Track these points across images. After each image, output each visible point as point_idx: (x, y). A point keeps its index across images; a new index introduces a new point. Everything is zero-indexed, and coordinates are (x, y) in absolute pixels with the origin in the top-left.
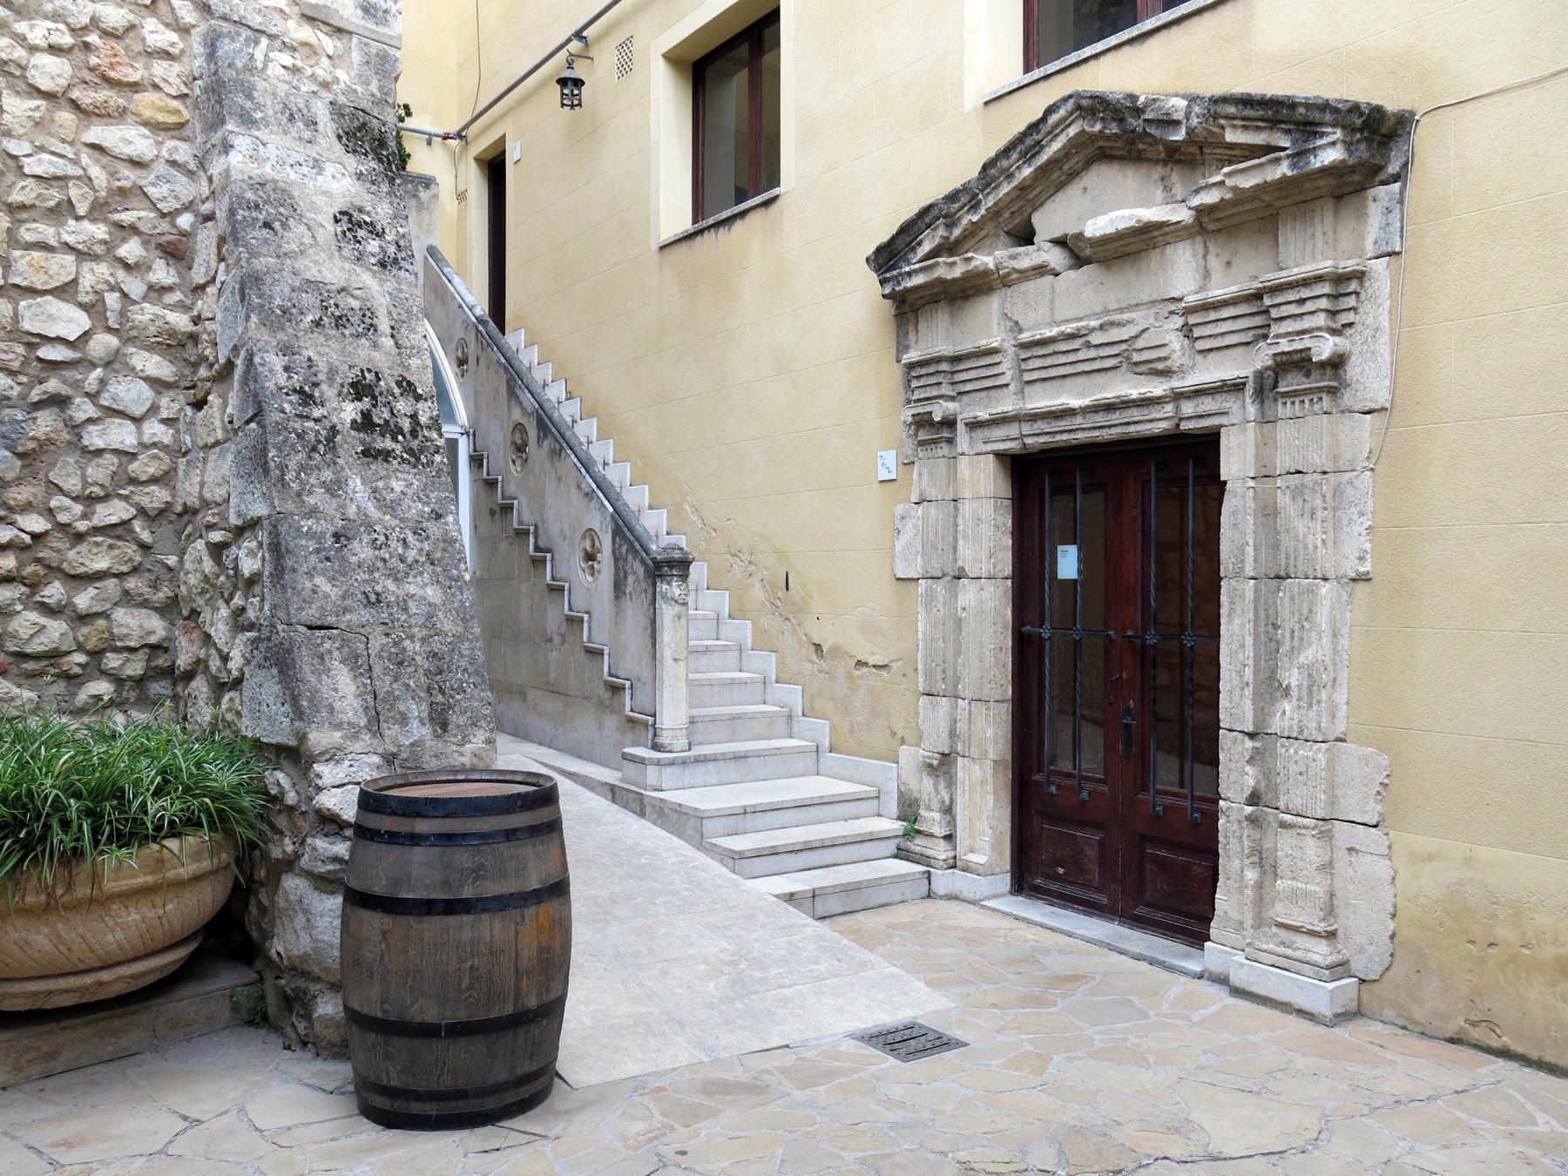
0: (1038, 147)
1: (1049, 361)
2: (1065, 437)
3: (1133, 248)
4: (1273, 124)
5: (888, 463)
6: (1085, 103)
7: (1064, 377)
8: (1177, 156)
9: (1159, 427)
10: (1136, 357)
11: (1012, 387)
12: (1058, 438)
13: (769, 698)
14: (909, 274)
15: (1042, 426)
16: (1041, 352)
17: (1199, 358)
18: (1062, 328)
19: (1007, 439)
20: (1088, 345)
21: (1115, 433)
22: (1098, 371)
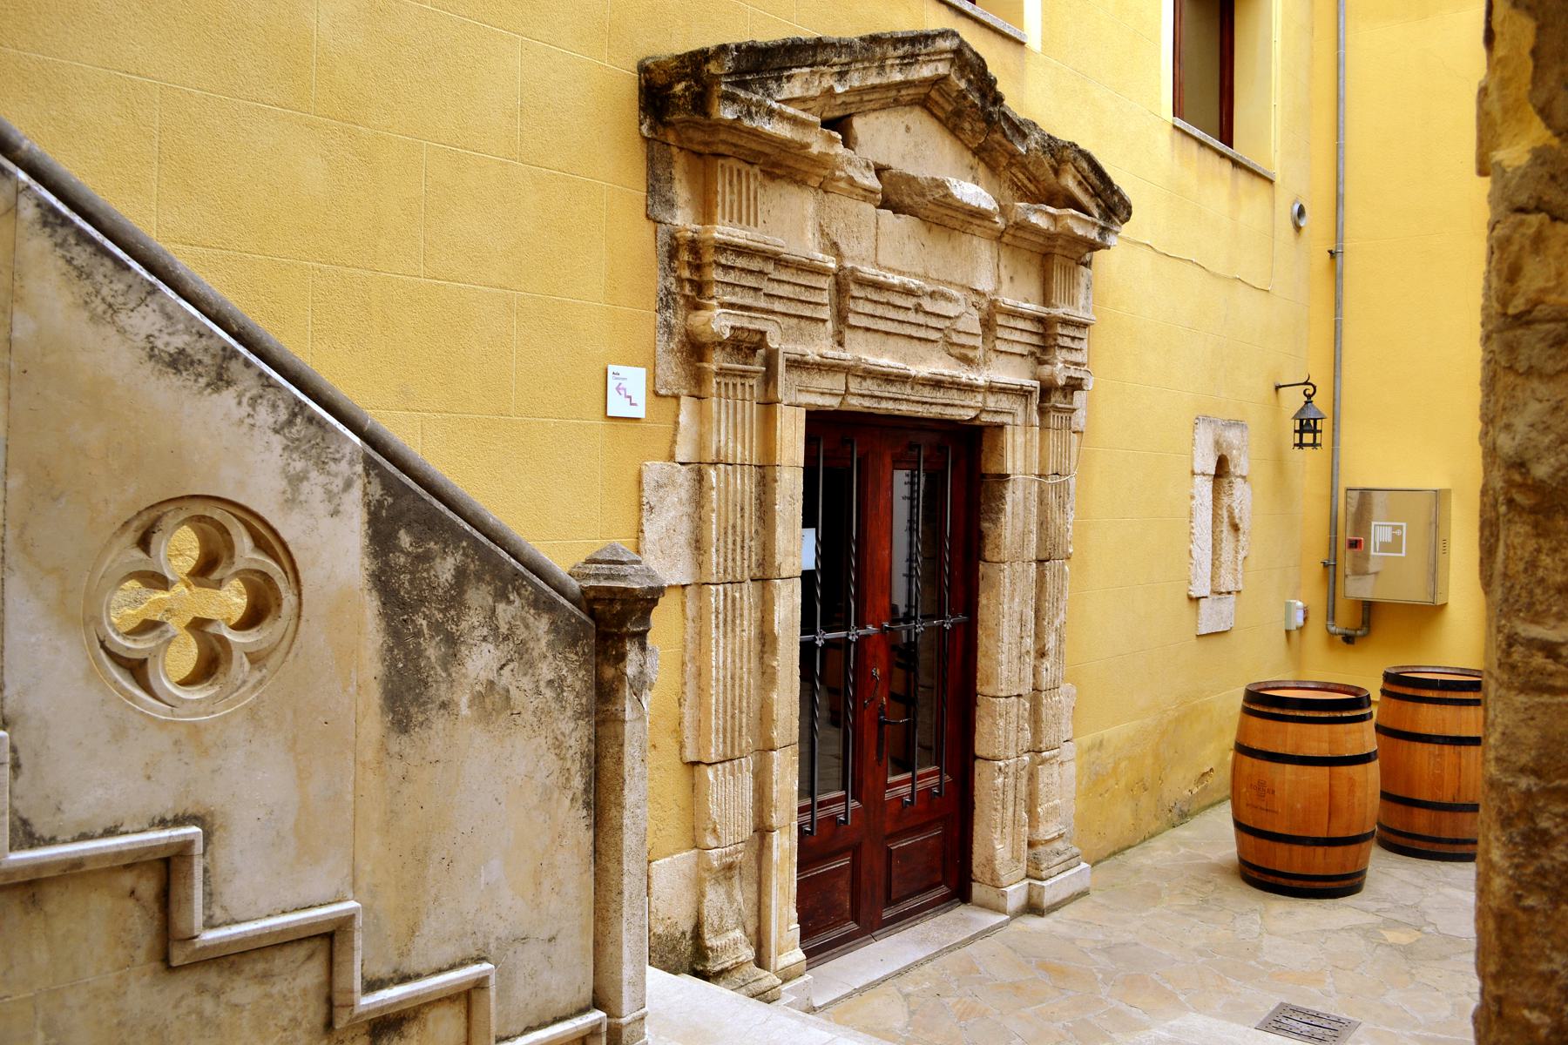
0: (909, 60)
1: (880, 311)
2: (890, 405)
3: (951, 223)
4: (1096, 195)
5: (630, 389)
6: (968, 54)
7: (887, 333)
8: (984, 155)
9: (968, 414)
10: (955, 338)
11: (829, 325)
12: (884, 405)
13: (219, 914)
14: (771, 113)
15: (870, 386)
16: (875, 297)
17: (993, 355)
18: (906, 279)
19: (825, 394)
20: (918, 309)
21: (934, 412)
22: (920, 339)
